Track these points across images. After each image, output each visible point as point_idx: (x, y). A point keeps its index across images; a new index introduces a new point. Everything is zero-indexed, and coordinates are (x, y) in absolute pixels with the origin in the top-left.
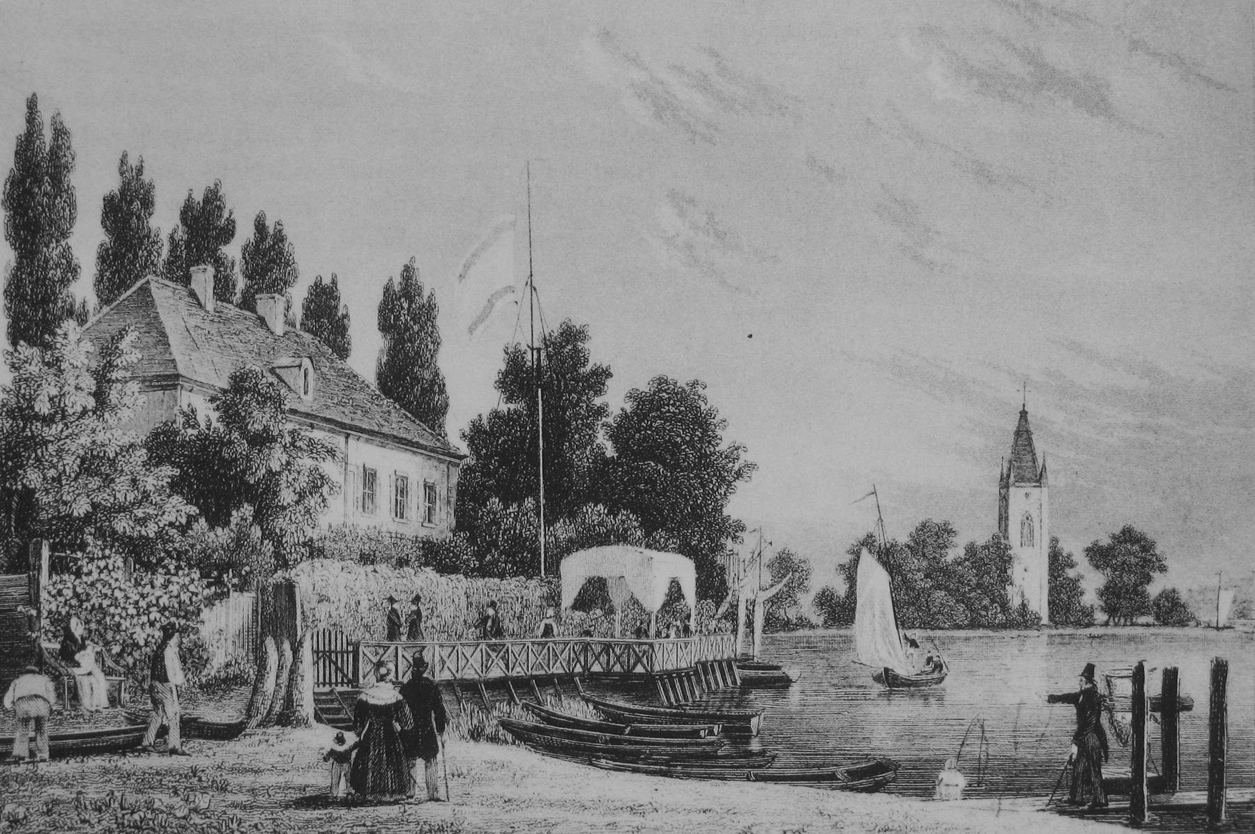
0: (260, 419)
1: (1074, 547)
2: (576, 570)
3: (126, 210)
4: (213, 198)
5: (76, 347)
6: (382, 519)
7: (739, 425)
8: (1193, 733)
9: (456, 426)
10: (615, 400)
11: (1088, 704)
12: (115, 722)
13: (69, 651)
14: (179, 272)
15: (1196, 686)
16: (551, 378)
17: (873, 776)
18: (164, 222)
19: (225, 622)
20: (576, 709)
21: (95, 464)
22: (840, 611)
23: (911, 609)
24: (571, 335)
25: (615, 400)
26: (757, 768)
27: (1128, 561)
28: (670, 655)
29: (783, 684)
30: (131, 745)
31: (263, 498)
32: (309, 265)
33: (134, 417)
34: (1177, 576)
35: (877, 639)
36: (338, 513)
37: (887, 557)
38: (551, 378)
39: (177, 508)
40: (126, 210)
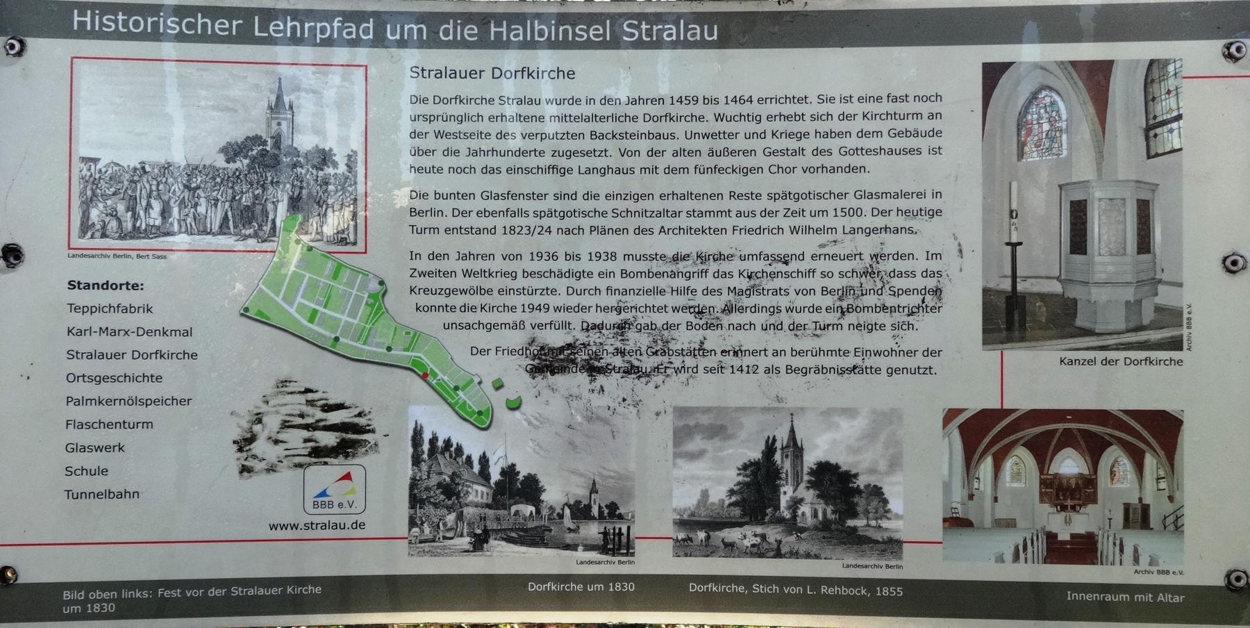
0: (457, 480)
1: (603, 505)
2: (514, 509)
3: (433, 441)
4: (449, 440)
5: (424, 467)
6: (479, 499)
7: (544, 481)
8: (624, 539)
9: (493, 481)
10: (521, 477)
11: (605, 534)
12: (431, 537)
13: (422, 523)
14: (442, 453)
15: (624, 530)
16: (509, 472)
17: (567, 547)
18: (440, 443)
19: (451, 518)
20: (513, 535)
21: (428, 489)
22: (561, 516)
23: (574, 516)
24: (513, 465)
25: (521, 477)
26: (546, 546)
27: (613, 507)
28: (531, 525)
29: (550, 530)
30: (434, 541)
31: (458, 496)
32: (466, 452)
33: (434, 480)
34: (265, 419)
35: (568, 522)
36: (471, 498)
37: (569, 506)
38: (509, 472)
39: (442, 497)
40: (433, 441)
